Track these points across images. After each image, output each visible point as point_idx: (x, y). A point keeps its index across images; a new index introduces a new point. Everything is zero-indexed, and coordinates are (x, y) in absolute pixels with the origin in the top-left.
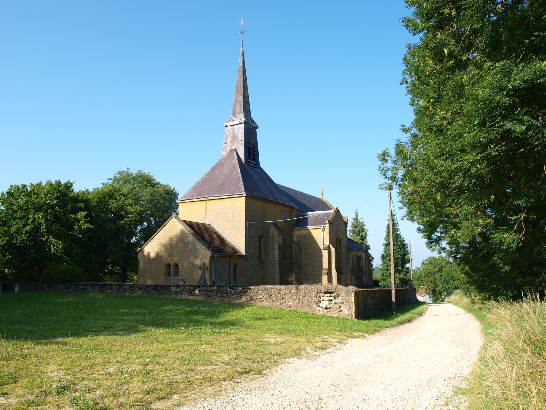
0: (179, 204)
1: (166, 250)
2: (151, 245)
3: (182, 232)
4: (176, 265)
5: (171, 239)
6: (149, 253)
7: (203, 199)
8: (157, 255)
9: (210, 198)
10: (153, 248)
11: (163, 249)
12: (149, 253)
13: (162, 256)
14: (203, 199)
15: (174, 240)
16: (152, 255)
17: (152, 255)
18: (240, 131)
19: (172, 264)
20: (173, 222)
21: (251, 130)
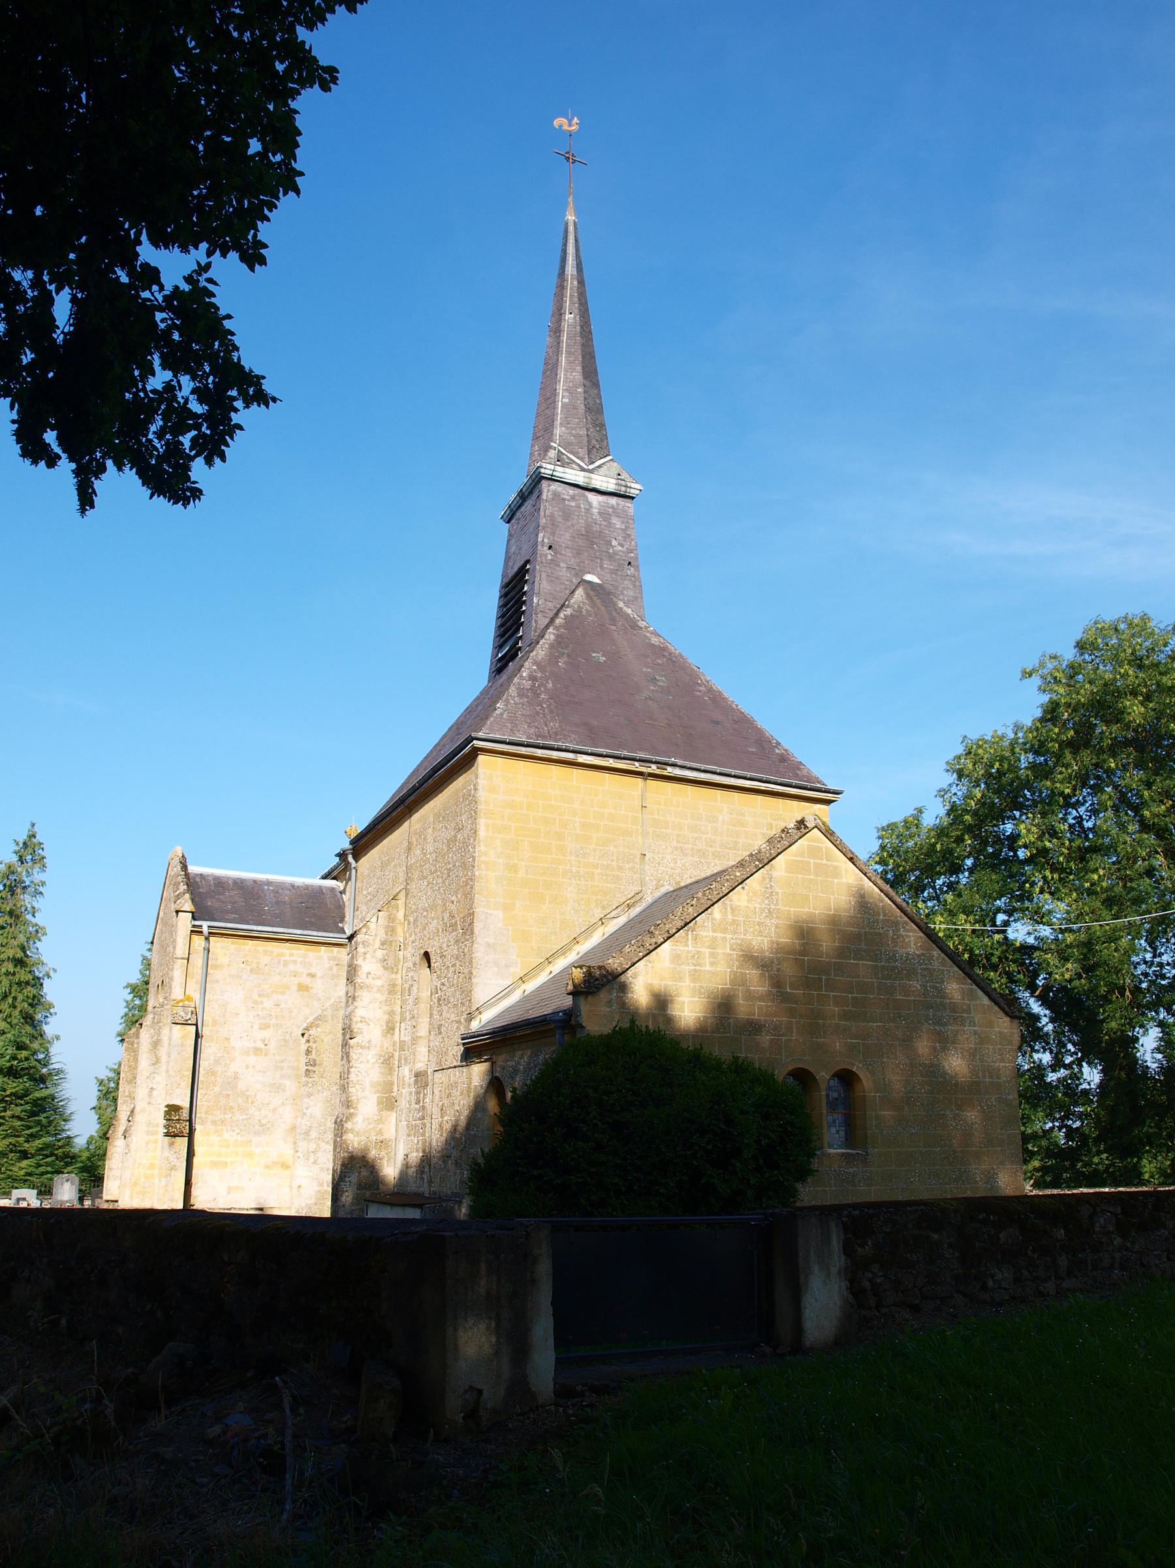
0: (481, 758)
1: (777, 983)
2: (676, 958)
3: (863, 904)
4: (846, 1078)
5: (804, 933)
6: (662, 1002)
7: (636, 766)
8: (723, 1006)
9: (582, 759)
10: (695, 976)
11: (757, 983)
12: (662, 1002)
13: (753, 1027)
14: (636, 766)
15: (827, 944)
16: (689, 1011)
17: (689, 1011)
18: (374, 855)
19: (823, 1076)
20: (814, 851)
21: (362, 844)
